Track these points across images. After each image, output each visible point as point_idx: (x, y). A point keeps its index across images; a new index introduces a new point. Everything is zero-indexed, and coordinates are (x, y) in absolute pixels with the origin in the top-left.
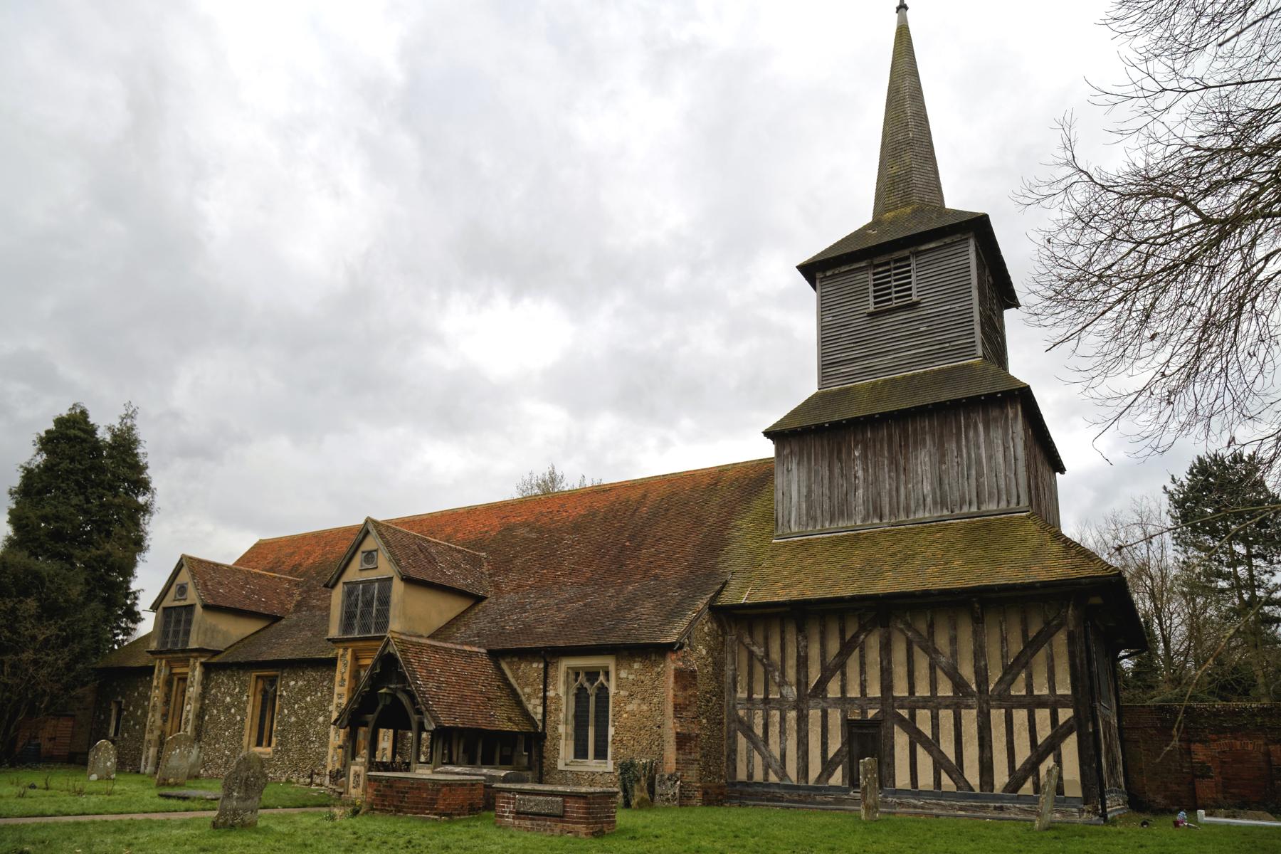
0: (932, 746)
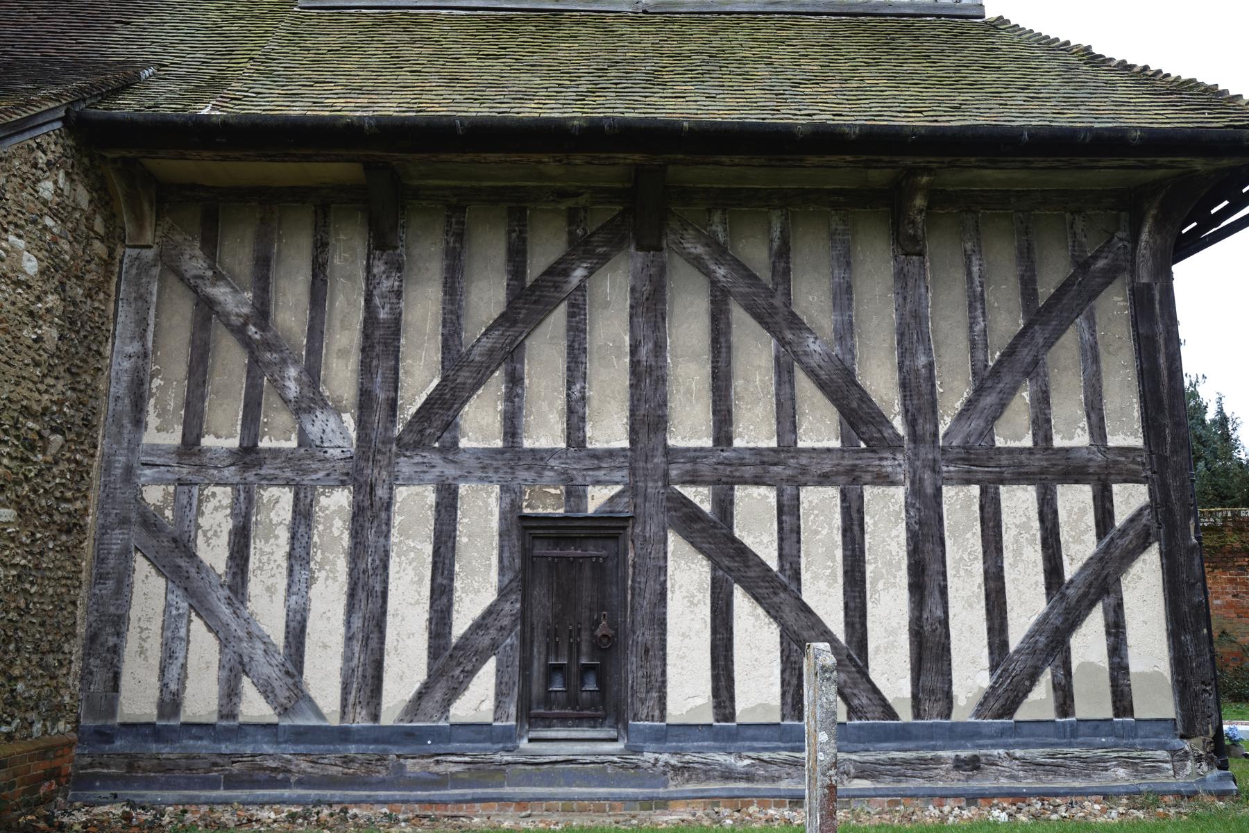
0: (779, 591)
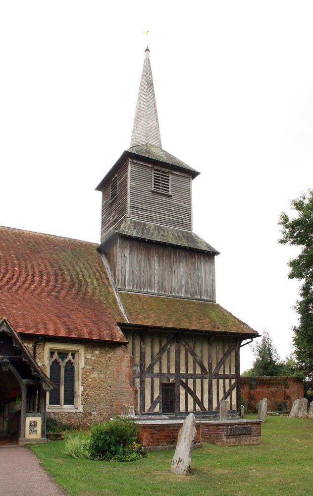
0: (193, 394)
